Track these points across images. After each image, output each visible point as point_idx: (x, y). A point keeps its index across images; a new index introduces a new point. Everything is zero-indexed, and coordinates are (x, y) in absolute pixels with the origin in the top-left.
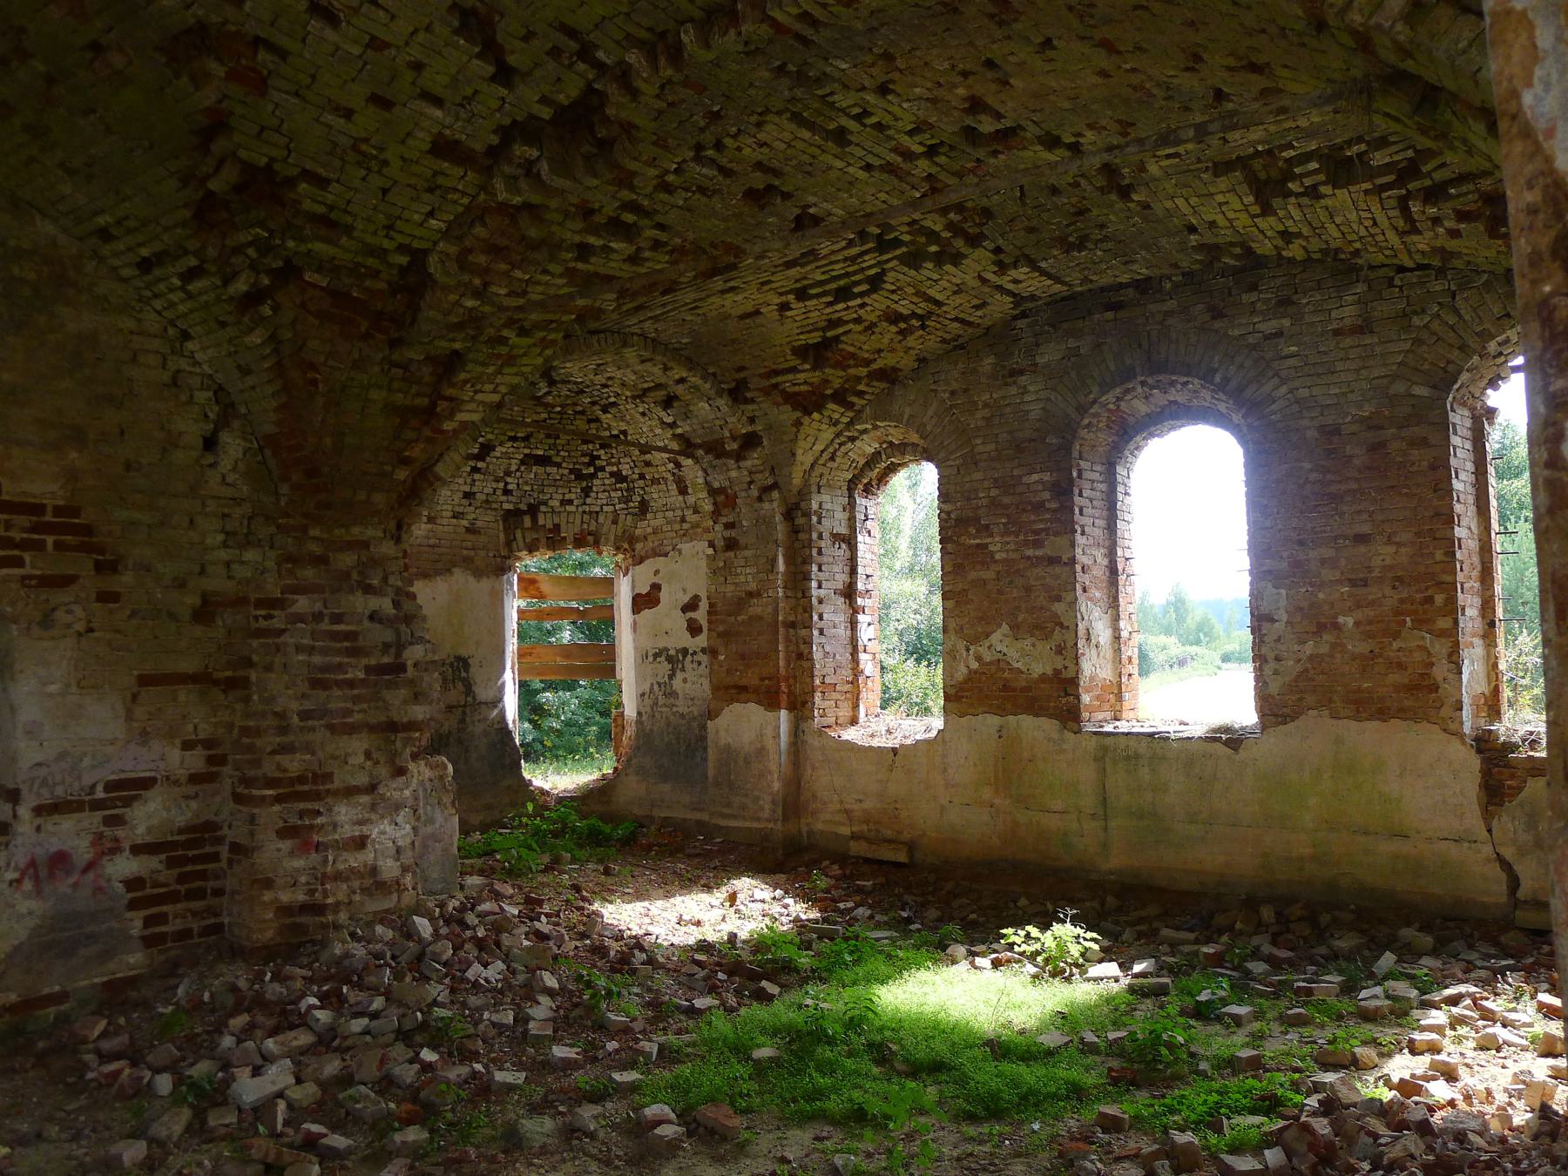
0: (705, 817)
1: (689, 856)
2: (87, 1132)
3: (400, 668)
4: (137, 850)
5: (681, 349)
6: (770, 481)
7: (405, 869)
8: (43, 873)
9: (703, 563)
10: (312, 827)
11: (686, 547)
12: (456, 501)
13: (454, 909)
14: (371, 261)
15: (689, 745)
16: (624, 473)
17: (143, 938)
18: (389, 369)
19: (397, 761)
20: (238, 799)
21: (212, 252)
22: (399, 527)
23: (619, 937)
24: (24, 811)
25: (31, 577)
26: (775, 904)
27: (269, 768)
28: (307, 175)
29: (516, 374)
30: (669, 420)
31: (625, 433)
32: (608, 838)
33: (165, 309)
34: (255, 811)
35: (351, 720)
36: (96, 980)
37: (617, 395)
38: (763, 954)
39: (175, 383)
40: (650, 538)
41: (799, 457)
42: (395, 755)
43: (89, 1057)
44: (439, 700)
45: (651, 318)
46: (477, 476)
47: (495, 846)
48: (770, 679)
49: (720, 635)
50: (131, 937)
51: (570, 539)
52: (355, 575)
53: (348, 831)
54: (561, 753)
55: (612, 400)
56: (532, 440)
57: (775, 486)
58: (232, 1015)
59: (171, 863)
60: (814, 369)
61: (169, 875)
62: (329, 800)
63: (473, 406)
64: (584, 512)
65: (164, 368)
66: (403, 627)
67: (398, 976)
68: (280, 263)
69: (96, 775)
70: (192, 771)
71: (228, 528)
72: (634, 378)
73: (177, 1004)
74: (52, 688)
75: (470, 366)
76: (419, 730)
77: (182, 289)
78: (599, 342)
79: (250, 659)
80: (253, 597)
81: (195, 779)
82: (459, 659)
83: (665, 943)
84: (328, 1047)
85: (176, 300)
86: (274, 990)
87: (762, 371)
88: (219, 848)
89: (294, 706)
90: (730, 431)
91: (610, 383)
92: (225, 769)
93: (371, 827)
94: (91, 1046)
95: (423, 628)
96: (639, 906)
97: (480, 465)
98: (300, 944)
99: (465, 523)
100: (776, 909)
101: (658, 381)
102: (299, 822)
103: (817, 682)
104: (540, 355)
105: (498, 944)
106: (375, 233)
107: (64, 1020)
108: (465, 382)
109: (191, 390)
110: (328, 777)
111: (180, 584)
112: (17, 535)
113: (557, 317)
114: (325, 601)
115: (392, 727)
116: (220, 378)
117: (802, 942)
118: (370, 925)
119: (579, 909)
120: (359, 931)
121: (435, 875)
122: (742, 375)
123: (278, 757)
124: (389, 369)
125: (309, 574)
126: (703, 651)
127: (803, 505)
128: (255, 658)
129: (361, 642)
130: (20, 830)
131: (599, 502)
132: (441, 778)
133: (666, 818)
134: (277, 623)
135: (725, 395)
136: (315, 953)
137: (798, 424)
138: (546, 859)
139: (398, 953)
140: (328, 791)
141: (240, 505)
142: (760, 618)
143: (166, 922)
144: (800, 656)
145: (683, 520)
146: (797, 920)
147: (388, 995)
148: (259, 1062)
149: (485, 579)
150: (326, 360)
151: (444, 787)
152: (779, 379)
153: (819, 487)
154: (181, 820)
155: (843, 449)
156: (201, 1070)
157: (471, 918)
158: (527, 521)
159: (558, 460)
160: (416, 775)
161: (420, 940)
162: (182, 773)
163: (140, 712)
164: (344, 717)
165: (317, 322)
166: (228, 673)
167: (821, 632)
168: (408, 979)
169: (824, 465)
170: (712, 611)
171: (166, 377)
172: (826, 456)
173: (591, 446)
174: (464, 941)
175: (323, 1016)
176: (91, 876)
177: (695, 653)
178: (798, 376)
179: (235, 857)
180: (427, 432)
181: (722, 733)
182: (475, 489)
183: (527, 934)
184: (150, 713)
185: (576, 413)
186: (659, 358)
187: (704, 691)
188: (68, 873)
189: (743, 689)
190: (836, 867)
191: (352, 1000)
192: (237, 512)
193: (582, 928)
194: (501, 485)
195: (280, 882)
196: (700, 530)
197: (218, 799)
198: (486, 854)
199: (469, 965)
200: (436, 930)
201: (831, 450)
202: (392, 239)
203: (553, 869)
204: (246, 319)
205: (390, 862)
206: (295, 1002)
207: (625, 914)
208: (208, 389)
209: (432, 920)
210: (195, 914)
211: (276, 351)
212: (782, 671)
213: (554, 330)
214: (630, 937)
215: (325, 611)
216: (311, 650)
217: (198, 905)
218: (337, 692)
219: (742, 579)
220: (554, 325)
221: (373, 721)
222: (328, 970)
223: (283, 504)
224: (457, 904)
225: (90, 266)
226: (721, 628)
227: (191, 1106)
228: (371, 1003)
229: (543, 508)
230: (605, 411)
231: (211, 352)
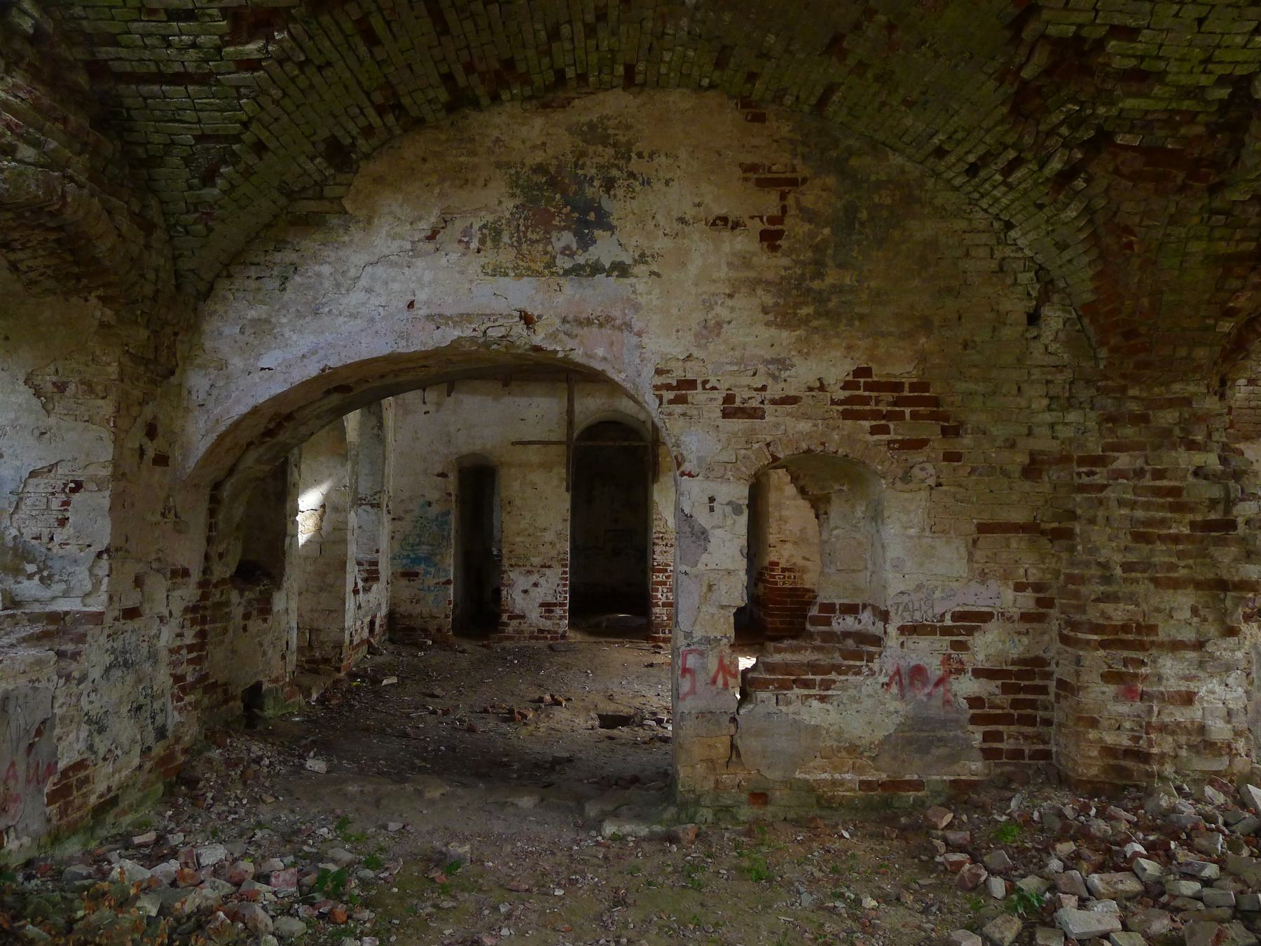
2: (934, 909)
3: (1232, 525)
4: (978, 673)
7: (1237, 734)
8: (906, 682)
10: (1136, 676)
14: (1187, 105)
17: (982, 750)
18: (1209, 218)
19: (1228, 622)
20: (1065, 640)
21: (1028, 140)
22: (1223, 382)
24: (892, 629)
25: (895, 441)
27: (1093, 614)
28: (1117, 31)
33: (990, 205)
34: (1081, 653)
35: (1176, 575)
36: (945, 778)
39: (1001, 269)
42: (1225, 614)
43: (938, 842)
50: (973, 747)
52: (1177, 431)
53: (1173, 685)
58: (1059, 840)
59: (1006, 689)
61: (1004, 700)
62: (1154, 652)
65: (992, 257)
66: (1232, 483)
67: (1233, 845)
68: (1092, 133)
69: (945, 606)
70: (1022, 611)
71: (1053, 392)
73: (1008, 815)
74: (912, 531)
77: (1004, 183)
79: (1074, 513)
80: (1076, 454)
81: (1025, 617)
84: (1156, 901)
85: (999, 195)
86: (1100, 827)
88: (1047, 682)
89: (1118, 558)
92: (1052, 611)
94: (940, 833)
98: (1125, 787)
102: (1124, 669)
106: (1191, 72)
107: (920, 804)
109: (1015, 273)
110: (1152, 629)
111: (1012, 445)
112: (884, 408)
114: (1146, 457)
115: (1222, 585)
116: (1040, 258)
123: (1102, 605)
124: (1209, 218)
125: (1129, 431)
128: (1079, 512)
129: (1185, 498)
130: (889, 644)
134: (1098, 479)
136: (1139, 799)
139: (1231, 820)
140: (1153, 643)
141: (1062, 372)
143: (1002, 740)
147: (1221, 862)
148: (1086, 895)
150: (1141, 221)
154: (1015, 652)
156: (1030, 884)
162: (1015, 612)
163: (979, 555)
164: (1168, 570)
165: (1131, 184)
166: (1055, 525)
168: (1245, 852)
171: (994, 265)
175: (1151, 867)
176: (941, 689)
179: (1062, 693)
184: (987, 557)
188: (924, 684)
191: (1181, 859)
192: (1060, 378)
195: (1104, 723)
197: (1046, 637)
202: (1211, 73)
204: (1061, 197)
205: (1220, 724)
206: (1122, 844)
208: (1029, 271)
210: (1026, 737)
211: (1091, 221)
215: (1147, 468)
216: (1133, 505)
217: (1028, 730)
218: (1159, 546)
222: (1154, 820)
223: (1102, 367)
225: (930, 183)
227: (1021, 916)
228: (1203, 868)
231: (1032, 236)
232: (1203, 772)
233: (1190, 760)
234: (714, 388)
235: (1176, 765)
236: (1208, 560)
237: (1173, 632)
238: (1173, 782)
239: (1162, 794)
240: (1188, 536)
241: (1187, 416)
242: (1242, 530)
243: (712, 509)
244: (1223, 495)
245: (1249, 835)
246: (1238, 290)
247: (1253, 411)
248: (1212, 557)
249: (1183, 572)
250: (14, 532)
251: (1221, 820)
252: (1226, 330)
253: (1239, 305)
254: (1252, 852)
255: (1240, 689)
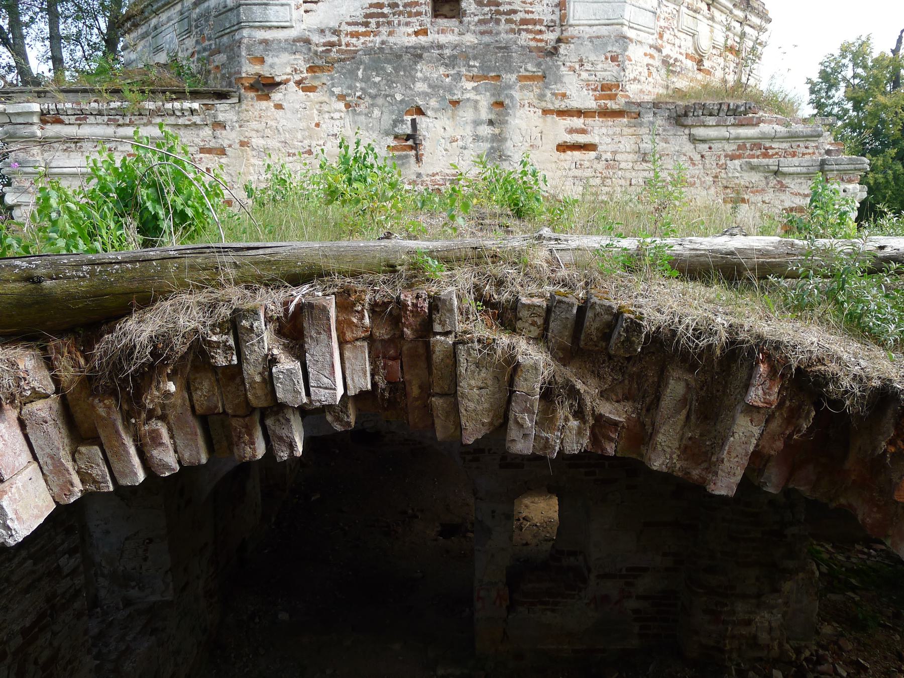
234: (495, 453)
243: (493, 517)
250: (122, 568)
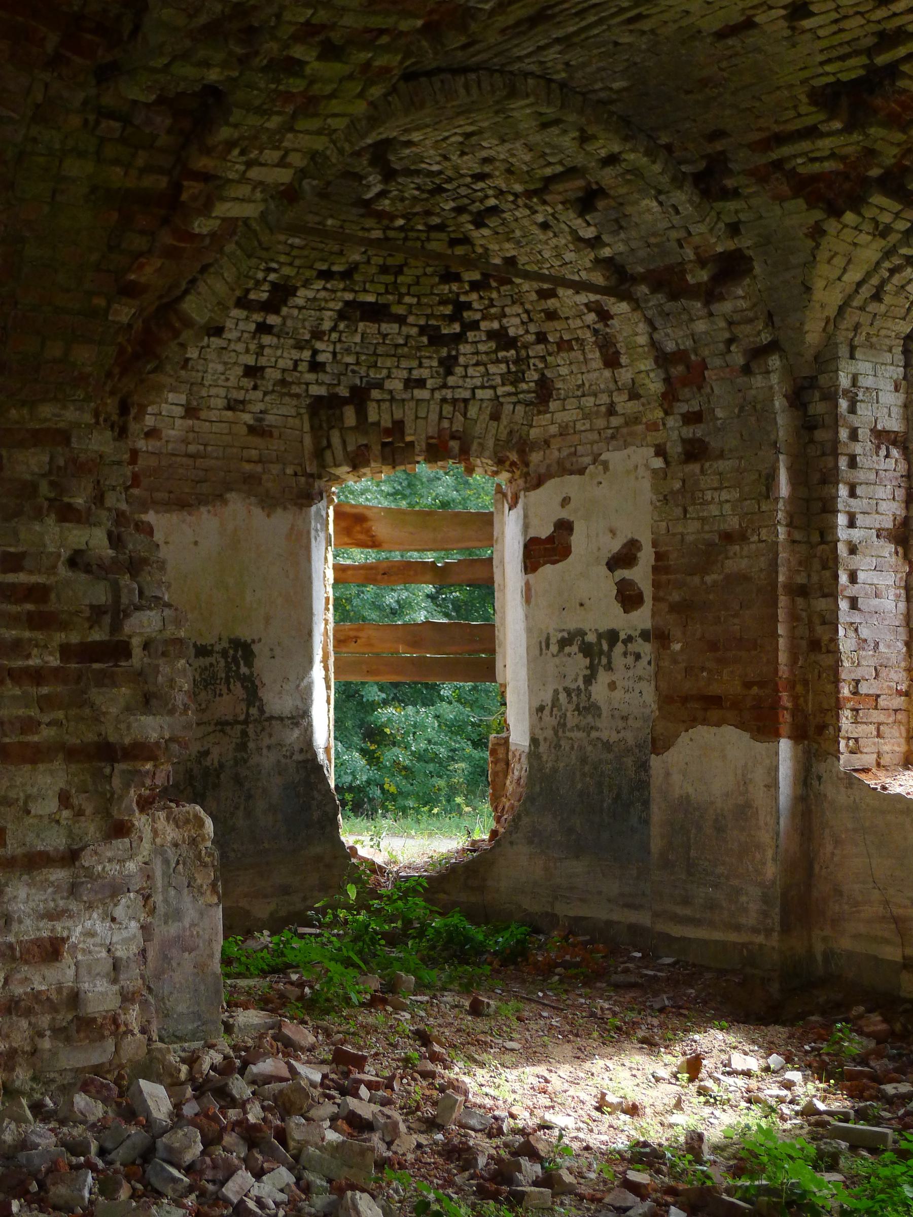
0: (643, 918)
1: (617, 987)
3: (122, 650)
5: (612, 102)
6: (765, 338)
7: (127, 998)
9: (646, 485)
11: (614, 457)
12: (233, 382)
13: (213, 1067)
15: (618, 796)
16: (512, 332)
18: (97, 123)
19: (115, 813)
22: (124, 408)
23: (494, 1131)
26: (769, 1078)
29: (319, 132)
30: (589, 233)
31: (511, 262)
32: (479, 950)
35: (36, 738)
37: (500, 193)
38: (751, 1179)
40: (555, 444)
41: (819, 294)
42: (110, 800)
44: (186, 708)
45: (558, 40)
46: (267, 340)
47: (290, 957)
48: (762, 684)
49: (674, 608)
51: (421, 446)
52: (44, 488)
54: (411, 803)
55: (492, 202)
56: (357, 277)
57: (773, 347)
60: (849, 129)
63: (244, 190)
64: (444, 400)
66: (125, 579)
72: (527, 158)
75: (237, 115)
76: (153, 758)
78: (467, 87)
82: (237, 643)
83: (576, 1145)
87: (757, 136)
90: (696, 248)
91: (487, 169)
93: (69, 923)
95: (160, 583)
96: (531, 1073)
97: (272, 319)
99: (247, 418)
100: (772, 1091)
101: (569, 163)
103: (845, 691)
104: (361, 95)
105: (282, 1136)
108: (231, 144)
113: (390, 22)
117: (821, 1154)
118: (66, 1090)
119: (426, 1075)
120: (48, 1101)
121: (181, 1008)
122: (719, 146)
126: (645, 635)
127: (823, 380)
129: (53, 605)
131: (469, 383)
132: (193, 842)
133: (577, 920)
135: (688, 186)
137: (817, 232)
138: (374, 983)
139: (109, 1145)
142: (745, 578)
144: (815, 645)
145: (611, 411)
146: (809, 1111)
149: (279, 511)
151: (199, 857)
152: (786, 151)
153: (852, 349)
155: (897, 280)
157: (239, 1087)
158: (350, 416)
159: (400, 310)
160: (147, 834)
161: (149, 1124)
164: (23, 732)
167: (854, 603)
168: (124, 1194)
169: (862, 309)
170: (661, 566)
172: (866, 292)
173: (455, 287)
174: (223, 1129)
177: (629, 639)
178: (820, 143)
180: (166, 238)
181: (676, 778)
182: (263, 361)
183: (333, 1119)
185: (431, 228)
186: (572, 118)
187: (645, 705)
189: (713, 702)
190: (876, 1017)
193: (429, 1111)
194: (307, 354)
196: (640, 428)
198: (274, 970)
199: (230, 1172)
200: (177, 1106)
201: (875, 281)
203: (384, 1002)
205: (102, 985)
207: (507, 1087)
209: (173, 1086)
212: (784, 671)
213: (386, 48)
214: (515, 1131)
219: (714, 510)
220: (384, 39)
221: (74, 741)
224: (218, 1058)
226: (675, 597)
229: (375, 394)
230: (479, 223)
232: (77, 1071)
233: (55, 1054)
235: (33, 1066)
236: (87, 711)
237: (30, 838)
238: (29, 1096)
239: (7, 1121)
240: (56, 670)
241: (61, 462)
242: (138, 657)
244: (110, 601)
245: (133, 1163)
246: (141, 254)
247: (190, 462)
248: (92, 706)
249: (46, 734)
251: (94, 1147)
252: (124, 319)
253: (143, 280)
254: (134, 1189)
255: (133, 924)
